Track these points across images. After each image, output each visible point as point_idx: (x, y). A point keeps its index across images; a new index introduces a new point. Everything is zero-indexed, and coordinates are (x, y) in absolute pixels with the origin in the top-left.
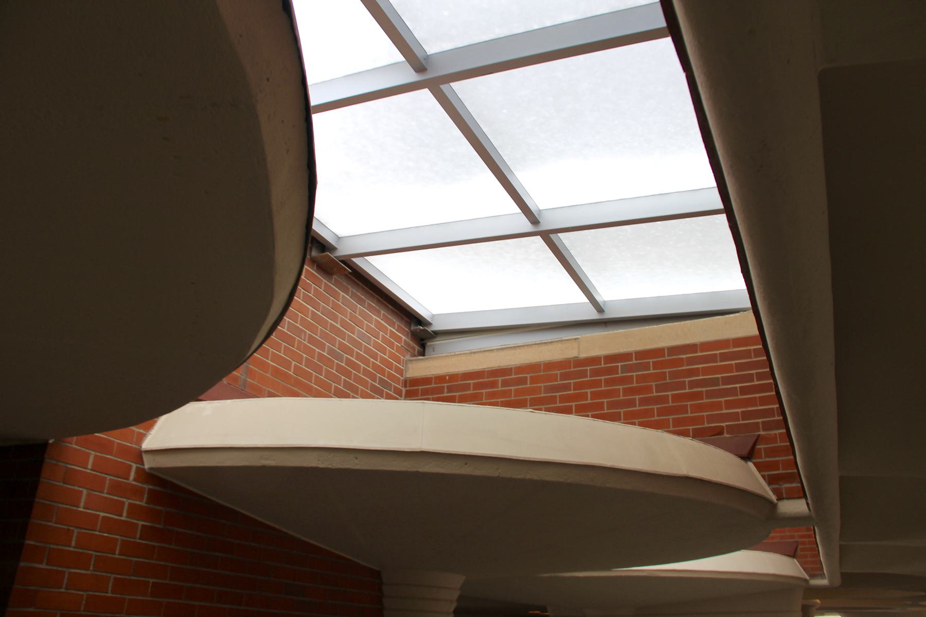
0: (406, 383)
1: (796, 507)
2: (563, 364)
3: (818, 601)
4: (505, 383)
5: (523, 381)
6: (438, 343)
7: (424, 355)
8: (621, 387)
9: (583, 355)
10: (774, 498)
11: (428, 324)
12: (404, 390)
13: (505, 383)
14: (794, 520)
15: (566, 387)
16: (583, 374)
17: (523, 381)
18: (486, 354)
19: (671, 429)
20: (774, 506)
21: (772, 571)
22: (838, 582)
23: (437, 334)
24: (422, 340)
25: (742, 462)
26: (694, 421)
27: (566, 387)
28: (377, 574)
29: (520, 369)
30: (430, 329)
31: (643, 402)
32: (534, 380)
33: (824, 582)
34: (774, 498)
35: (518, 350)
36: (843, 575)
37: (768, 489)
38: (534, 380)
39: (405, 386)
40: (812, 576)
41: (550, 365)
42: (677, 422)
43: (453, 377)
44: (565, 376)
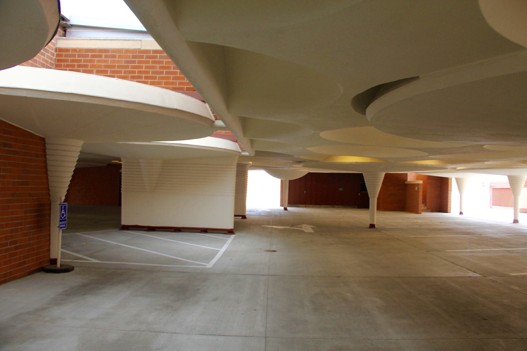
0: (56, 50)
1: (219, 123)
2: (134, 51)
3: (251, 163)
4: (106, 56)
5: (114, 56)
6: (73, 30)
7: (65, 36)
8: (158, 65)
9: (143, 48)
10: (214, 119)
11: (68, 21)
12: (55, 54)
13: (106, 56)
14: (220, 128)
15: (134, 62)
16: (142, 57)
17: (114, 56)
18: (98, 41)
19: (163, 86)
20: (213, 122)
21: (224, 147)
22: (253, 154)
23: (72, 26)
24: (64, 28)
25: (203, 103)
26: (172, 83)
27: (134, 62)
28: (43, 139)
29: (114, 51)
30: (69, 23)
31: (167, 73)
32: (120, 57)
33: (246, 154)
34: (213, 119)
35: (113, 42)
36: (256, 151)
37: (212, 115)
38: (120, 57)
39: (56, 52)
40: (243, 151)
41: (127, 51)
42: (166, 83)
43: (81, 50)
44: (134, 57)
